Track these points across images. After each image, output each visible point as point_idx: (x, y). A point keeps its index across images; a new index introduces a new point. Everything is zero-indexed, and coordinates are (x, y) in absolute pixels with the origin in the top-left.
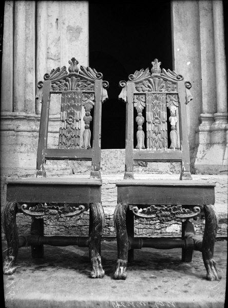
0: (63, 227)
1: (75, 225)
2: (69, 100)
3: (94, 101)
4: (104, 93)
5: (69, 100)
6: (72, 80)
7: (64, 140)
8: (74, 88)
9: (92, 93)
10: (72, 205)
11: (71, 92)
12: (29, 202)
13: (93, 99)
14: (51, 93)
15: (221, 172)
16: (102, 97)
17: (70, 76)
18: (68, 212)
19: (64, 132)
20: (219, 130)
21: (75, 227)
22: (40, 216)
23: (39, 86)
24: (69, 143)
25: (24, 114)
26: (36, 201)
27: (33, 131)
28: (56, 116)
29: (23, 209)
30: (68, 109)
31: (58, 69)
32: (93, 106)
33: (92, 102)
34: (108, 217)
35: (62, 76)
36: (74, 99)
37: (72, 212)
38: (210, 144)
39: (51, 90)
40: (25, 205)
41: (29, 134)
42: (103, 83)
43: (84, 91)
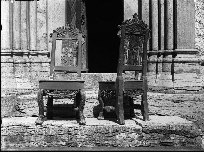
0: (44, 136)
1: (52, 134)
2: (66, 43)
3: (78, 44)
4: (83, 40)
5: (66, 43)
6: (67, 33)
7: (64, 62)
8: (68, 37)
9: (77, 40)
10: (70, 90)
11: (67, 39)
12: (50, 89)
13: (78, 42)
14: (56, 39)
15: (153, 90)
16: (82, 42)
17: (66, 31)
18: (69, 94)
19: (64, 58)
20: (153, 62)
21: (52, 135)
22: (55, 96)
23: (51, 36)
24: (66, 64)
25: (20, 51)
26: (54, 89)
27: (25, 63)
28: (43, 52)
29: (47, 93)
30: (65, 47)
31: (60, 28)
32: (78, 46)
33: (77, 44)
34: (76, 128)
35: (62, 31)
36: (68, 42)
37: (71, 94)
38: (63, 27)
39: (57, 38)
40: (48, 91)
41: (24, 65)
42: (82, 35)
43: (73, 39)
